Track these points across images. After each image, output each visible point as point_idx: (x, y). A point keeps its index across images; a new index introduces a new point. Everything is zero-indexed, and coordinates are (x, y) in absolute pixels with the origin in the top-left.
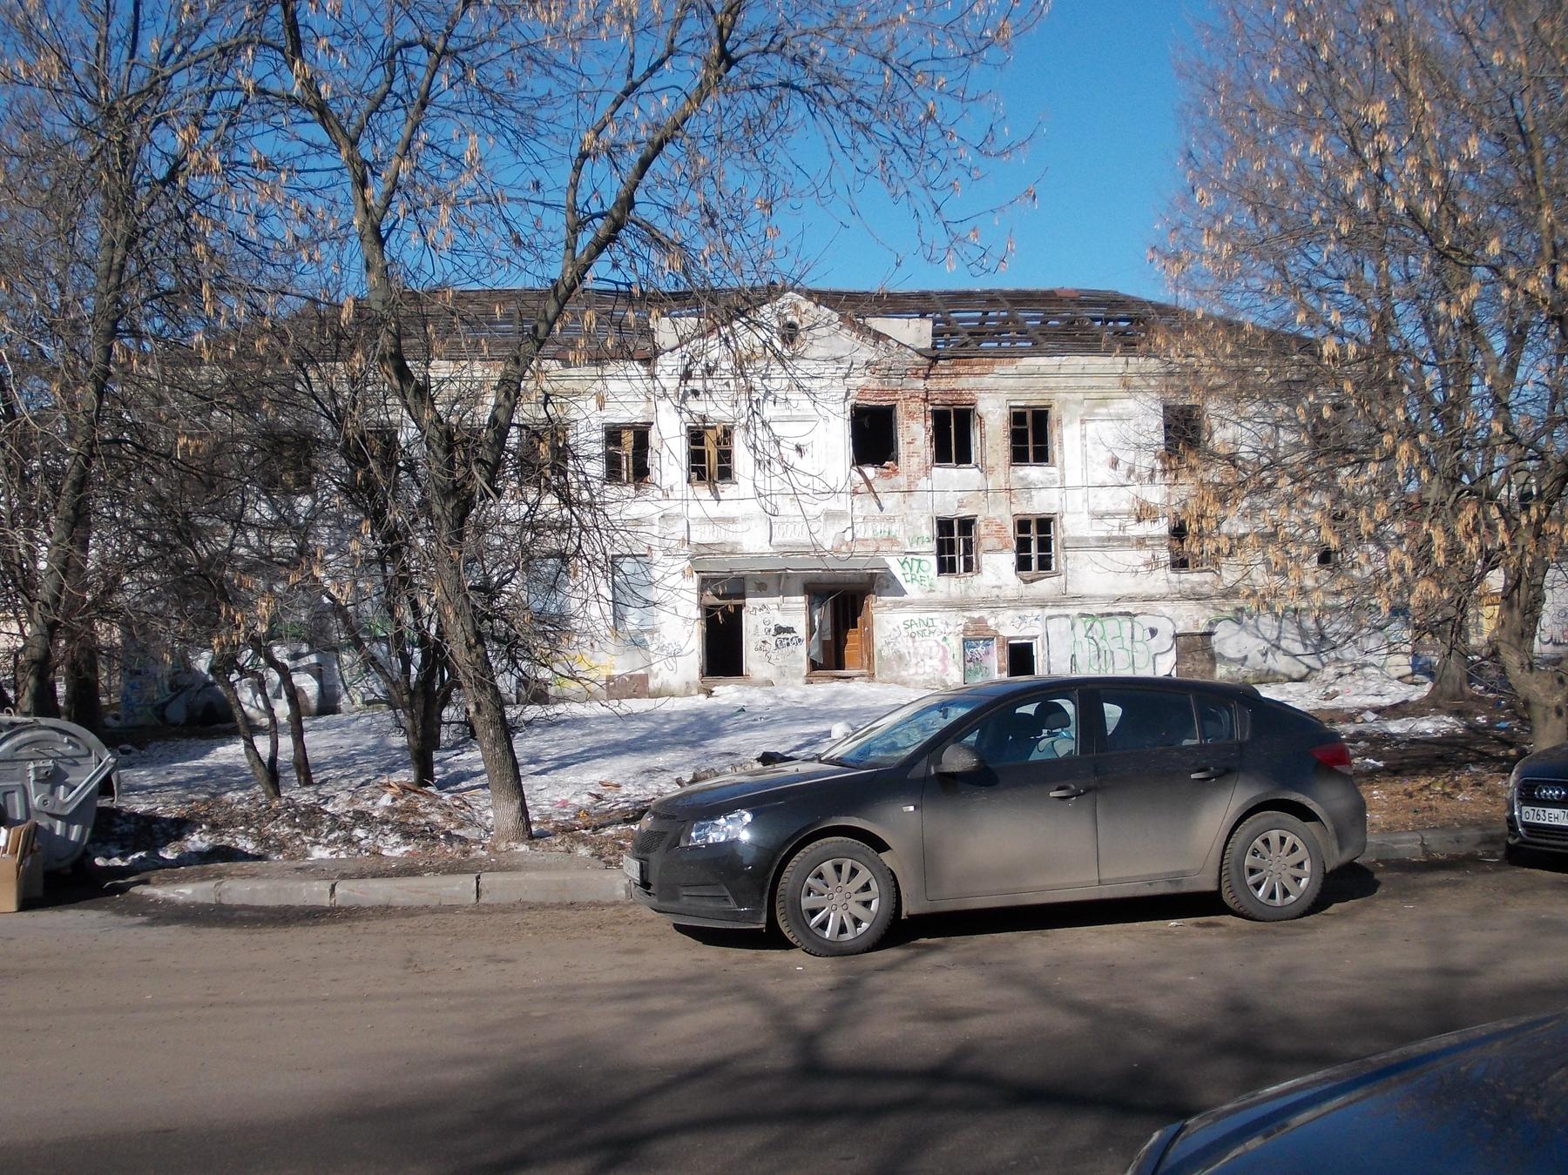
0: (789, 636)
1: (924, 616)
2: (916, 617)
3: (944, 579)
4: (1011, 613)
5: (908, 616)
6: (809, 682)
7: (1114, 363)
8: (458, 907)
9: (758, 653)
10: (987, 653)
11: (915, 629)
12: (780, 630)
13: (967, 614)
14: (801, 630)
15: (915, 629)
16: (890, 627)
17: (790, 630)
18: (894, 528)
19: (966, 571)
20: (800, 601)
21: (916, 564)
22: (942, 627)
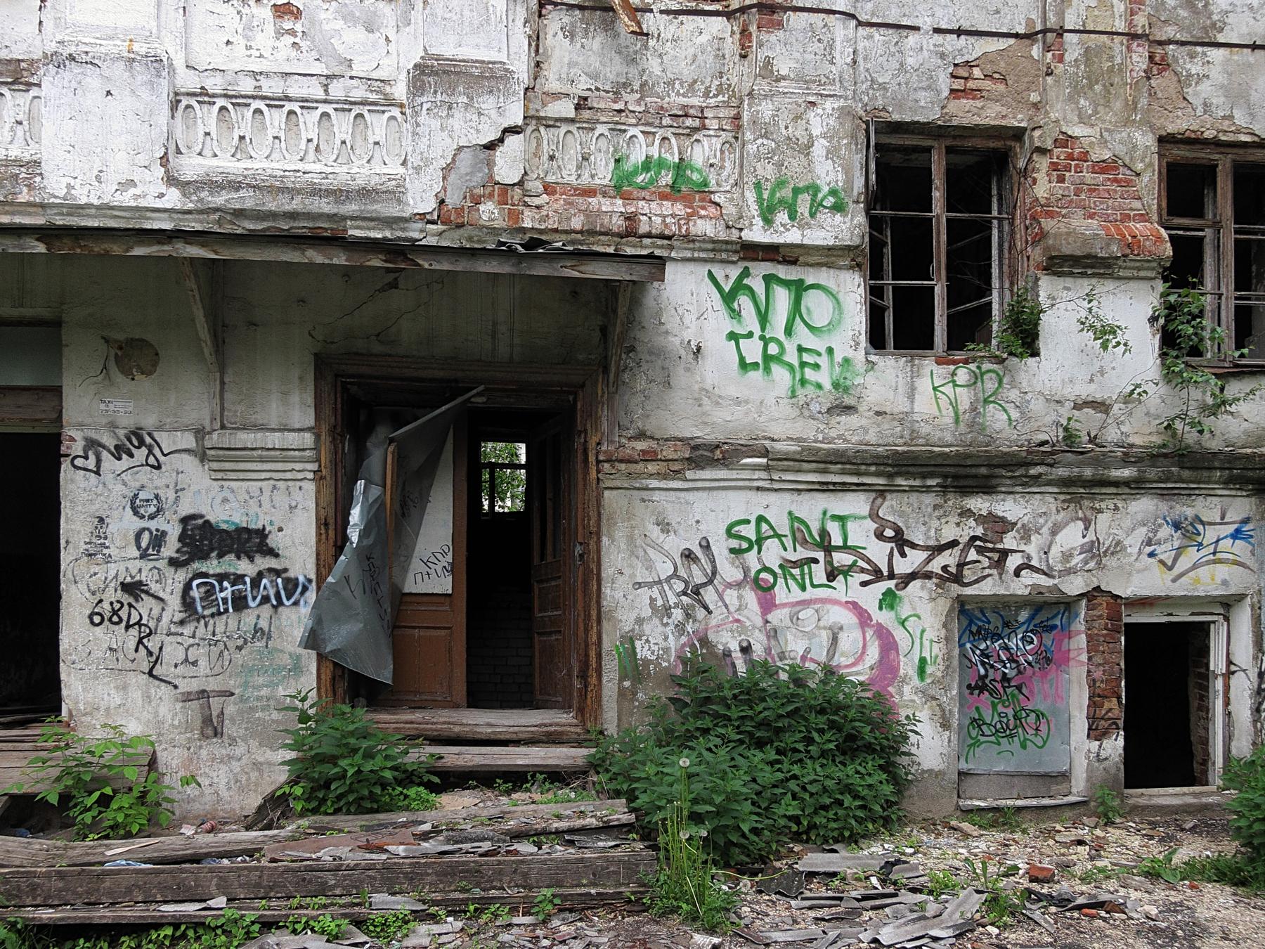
0: (245, 567)
1: (812, 509)
2: (777, 508)
3: (891, 366)
4: (1143, 506)
5: (742, 505)
6: (1018, 134)
7: (605, 540)
8: (841, 313)
9: (104, 636)
10: (1046, 659)
12: (201, 539)
13: (979, 504)
14: (298, 544)
15: (773, 554)
16: (675, 544)
17: (251, 541)
18: (703, 152)
19: (955, 343)
20: (289, 417)
21: (782, 297)
22: (879, 552)
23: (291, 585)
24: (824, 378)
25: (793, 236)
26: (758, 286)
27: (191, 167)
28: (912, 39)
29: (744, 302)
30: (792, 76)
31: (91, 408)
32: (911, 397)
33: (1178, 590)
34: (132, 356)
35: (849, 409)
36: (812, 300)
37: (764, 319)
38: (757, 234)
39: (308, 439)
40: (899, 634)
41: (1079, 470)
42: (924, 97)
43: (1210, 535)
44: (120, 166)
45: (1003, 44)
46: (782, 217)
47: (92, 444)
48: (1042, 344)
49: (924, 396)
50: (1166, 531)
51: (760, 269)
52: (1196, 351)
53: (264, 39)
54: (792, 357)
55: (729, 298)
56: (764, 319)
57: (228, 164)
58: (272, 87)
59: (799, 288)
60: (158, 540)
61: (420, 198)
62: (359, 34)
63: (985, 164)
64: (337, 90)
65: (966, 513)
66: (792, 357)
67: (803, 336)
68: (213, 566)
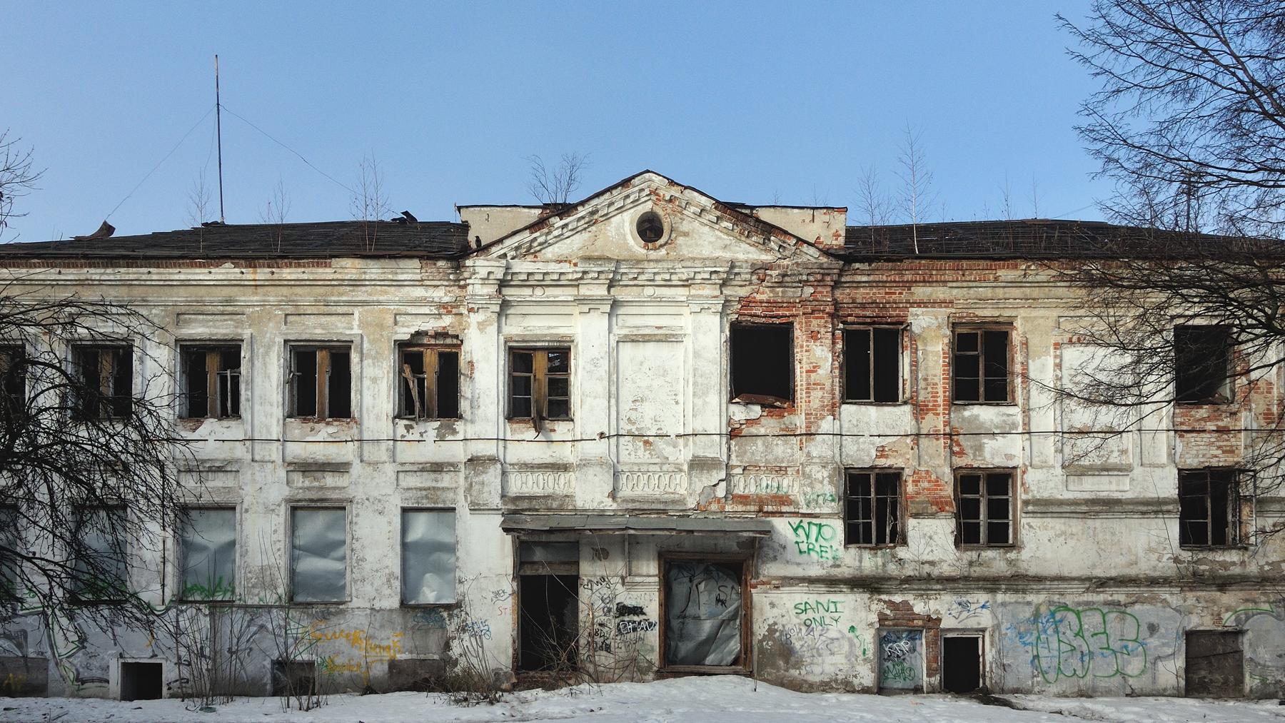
0: (636, 618)
11: (810, 614)
12: (623, 610)
15: (810, 614)
17: (638, 611)
21: (814, 530)
23: (650, 624)
24: (829, 555)
25: (817, 511)
26: (806, 526)
27: (626, 491)
28: (862, 439)
29: (800, 531)
30: (197, 560)
31: (588, 569)
32: (860, 561)
33: (960, 626)
34: (601, 554)
35: (839, 566)
36: (823, 529)
37: (808, 537)
38: (804, 511)
39: (657, 579)
40: (856, 640)
41: (927, 582)
42: (867, 459)
43: (973, 607)
44: (598, 497)
45: (895, 439)
46: (813, 504)
47: (590, 581)
48: (909, 540)
49: (868, 562)
50: (955, 606)
51: (806, 520)
52: (1063, 394)
53: (641, 452)
54: (818, 549)
55: (795, 530)
56: (808, 537)
57: (638, 492)
58: (644, 468)
59: (820, 526)
60: (610, 610)
61: (691, 504)
62: (671, 449)
63: (890, 480)
64: (665, 468)
65: (880, 600)
66: (818, 549)
67: (821, 541)
68: (626, 618)
